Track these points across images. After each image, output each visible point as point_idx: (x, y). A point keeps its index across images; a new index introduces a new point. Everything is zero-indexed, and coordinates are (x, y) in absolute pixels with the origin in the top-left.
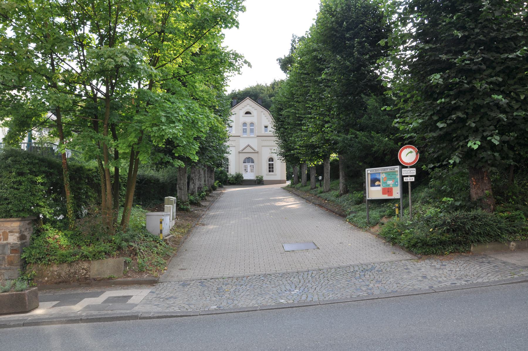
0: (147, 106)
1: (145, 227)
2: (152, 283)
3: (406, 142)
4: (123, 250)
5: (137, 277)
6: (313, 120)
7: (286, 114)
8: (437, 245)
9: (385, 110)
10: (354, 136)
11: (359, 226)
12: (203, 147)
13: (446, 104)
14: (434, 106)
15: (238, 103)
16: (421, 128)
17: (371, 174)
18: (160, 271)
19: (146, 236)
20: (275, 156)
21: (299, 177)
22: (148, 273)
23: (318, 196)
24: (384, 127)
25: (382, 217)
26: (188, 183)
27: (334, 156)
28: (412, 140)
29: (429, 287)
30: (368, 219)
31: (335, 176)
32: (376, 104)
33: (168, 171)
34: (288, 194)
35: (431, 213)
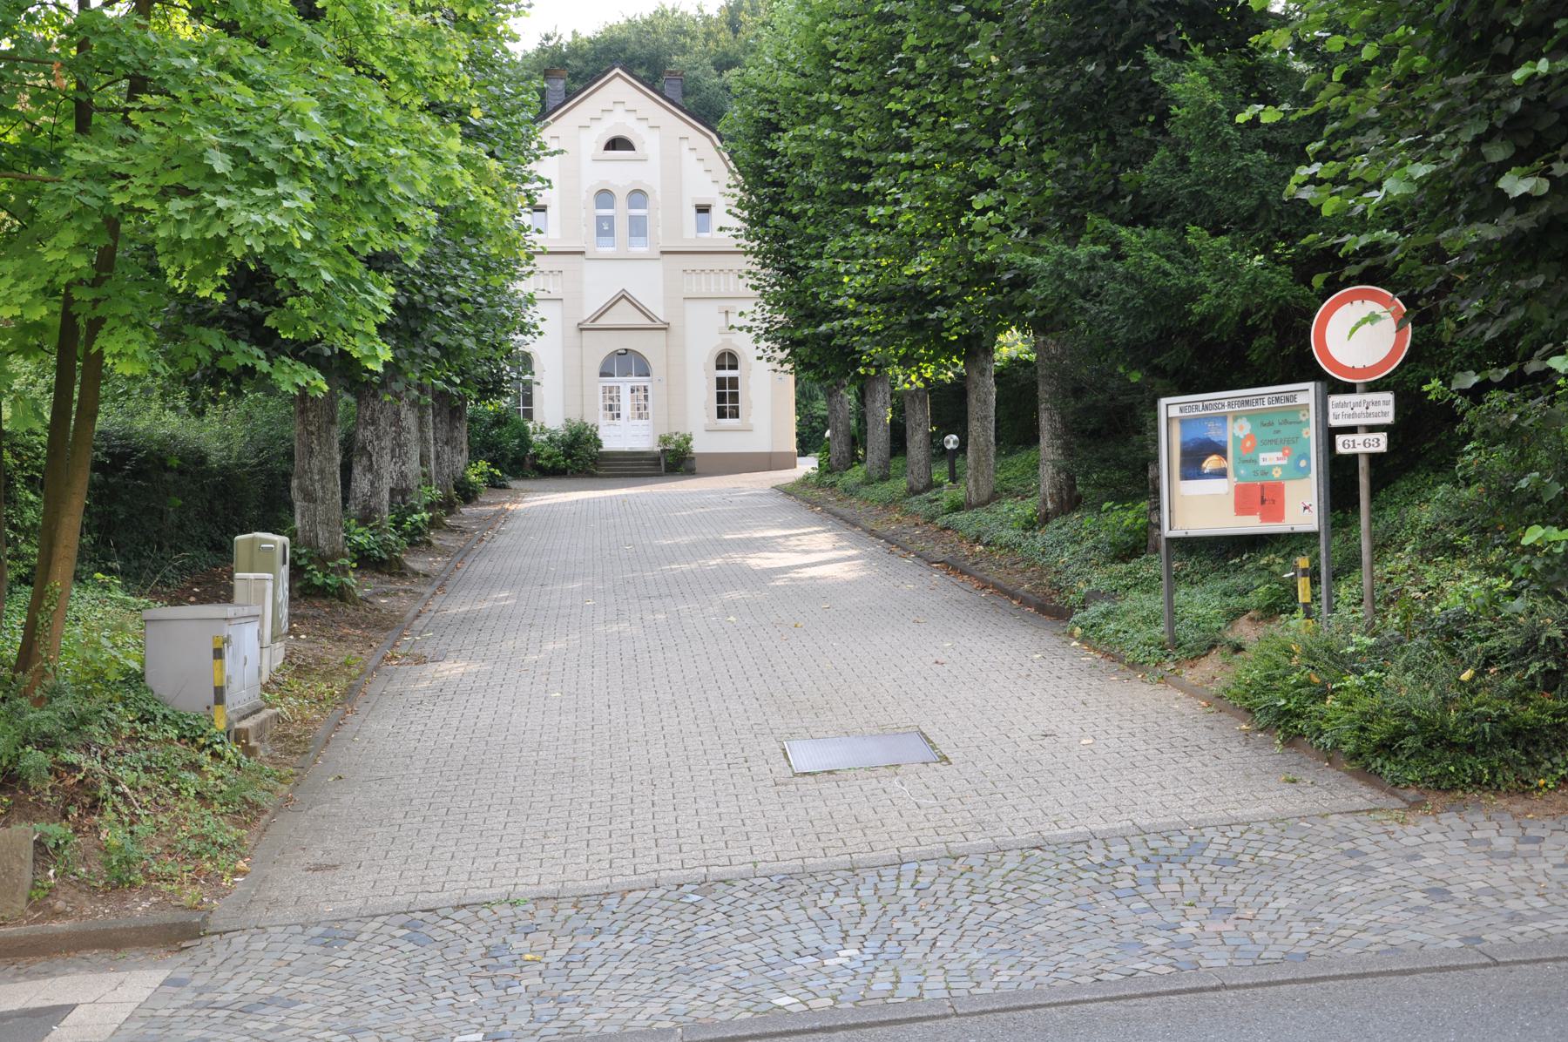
0: (131, 98)
1: (140, 677)
2: (178, 935)
3: (1352, 270)
4: (26, 788)
5: (101, 914)
6: (916, 176)
7: (794, 148)
8: (1495, 743)
9: (1255, 122)
10: (1103, 249)
11: (1131, 657)
12: (412, 305)
13: (1555, 82)
14: (1493, 95)
15: (570, 95)
16: (1423, 206)
17: (1183, 421)
18: (212, 880)
19: (143, 720)
20: (744, 345)
21: (857, 440)
22: (157, 892)
24: (1246, 203)
25: (1234, 615)
26: (346, 470)
27: (1012, 344)
28: (1379, 260)
29: (1465, 939)
30: (1172, 624)
31: (1017, 431)
32: (1213, 98)
33: (249, 416)
34: (806, 514)
35: (1466, 598)
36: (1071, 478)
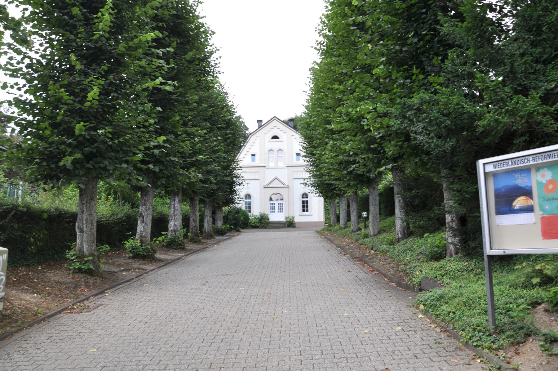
23: (360, 242)
36: (408, 224)
